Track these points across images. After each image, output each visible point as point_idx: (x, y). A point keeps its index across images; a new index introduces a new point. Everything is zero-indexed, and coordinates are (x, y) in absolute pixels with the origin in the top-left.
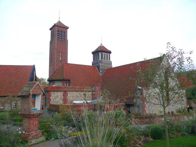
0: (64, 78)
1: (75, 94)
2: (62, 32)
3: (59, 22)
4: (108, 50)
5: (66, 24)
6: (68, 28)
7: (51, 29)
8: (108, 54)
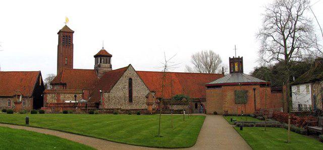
6: (73, 32)
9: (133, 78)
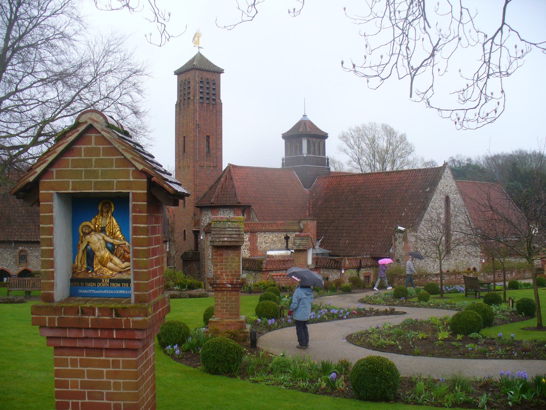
0: (240, 201)
1: (270, 237)
2: (208, 83)
3: (200, 57)
4: (322, 132)
5: (216, 61)
7: (178, 73)
8: (319, 140)
9: (451, 196)
